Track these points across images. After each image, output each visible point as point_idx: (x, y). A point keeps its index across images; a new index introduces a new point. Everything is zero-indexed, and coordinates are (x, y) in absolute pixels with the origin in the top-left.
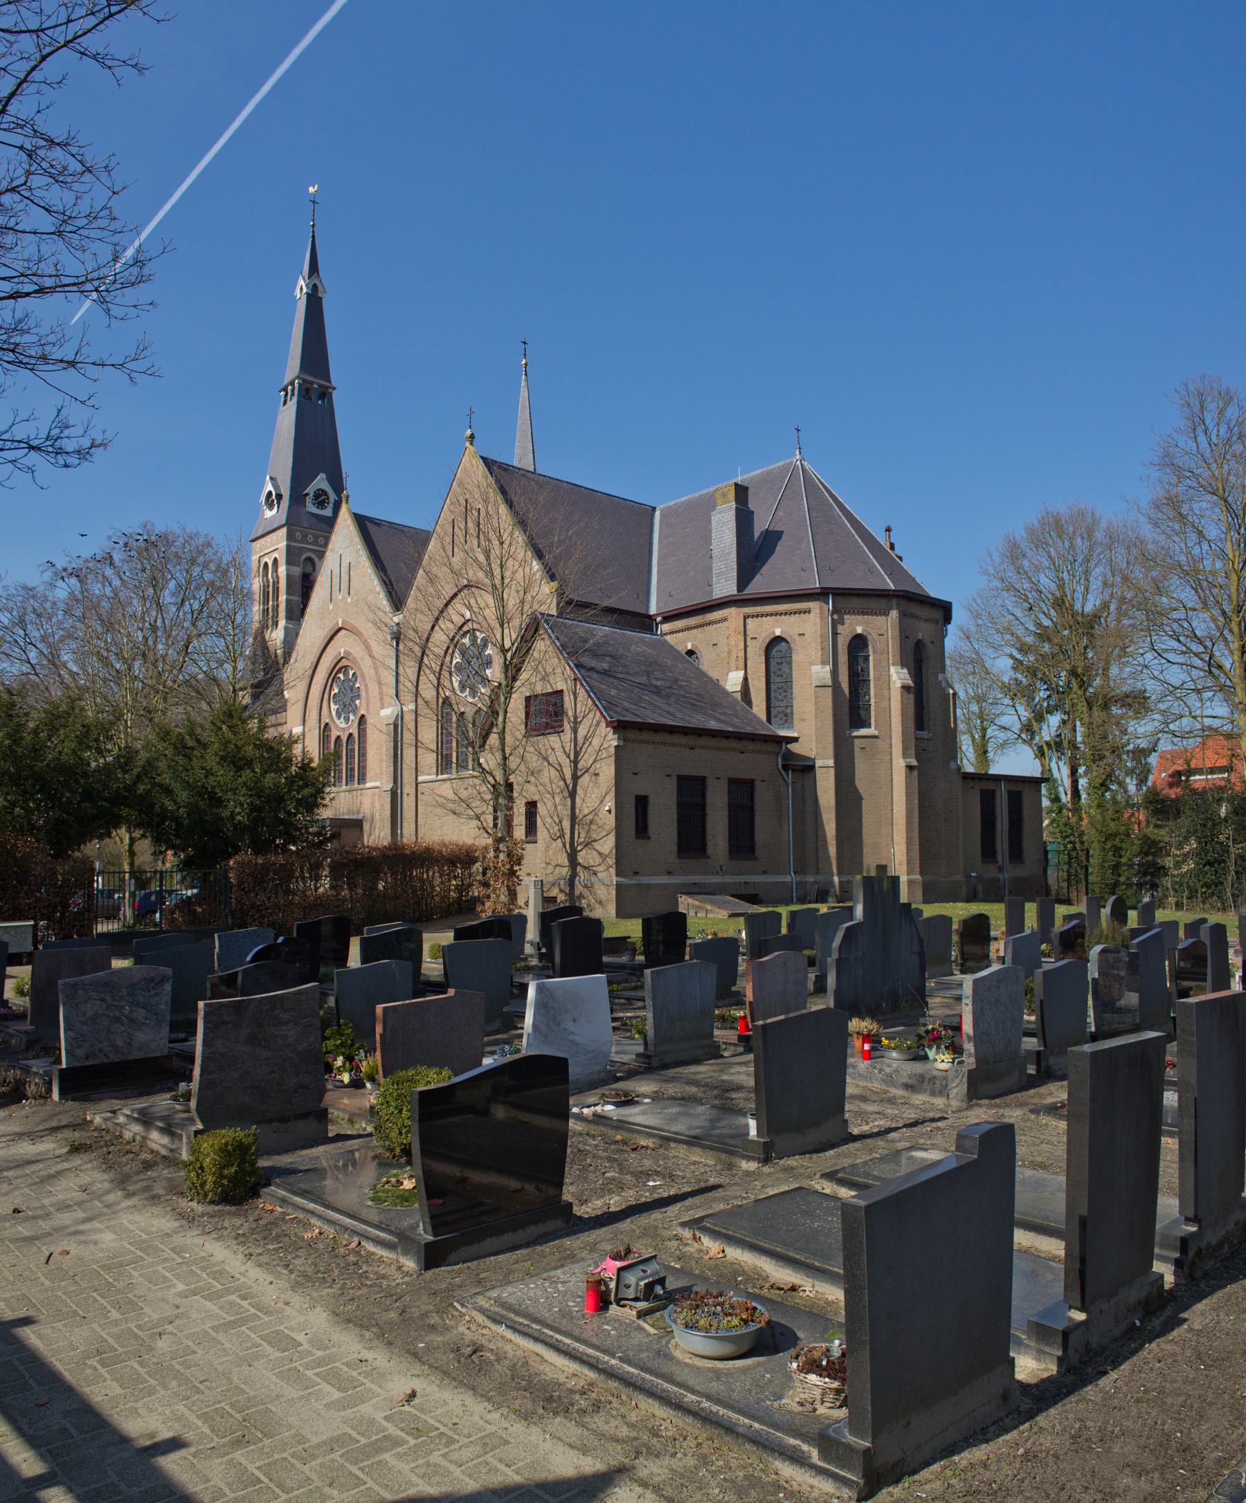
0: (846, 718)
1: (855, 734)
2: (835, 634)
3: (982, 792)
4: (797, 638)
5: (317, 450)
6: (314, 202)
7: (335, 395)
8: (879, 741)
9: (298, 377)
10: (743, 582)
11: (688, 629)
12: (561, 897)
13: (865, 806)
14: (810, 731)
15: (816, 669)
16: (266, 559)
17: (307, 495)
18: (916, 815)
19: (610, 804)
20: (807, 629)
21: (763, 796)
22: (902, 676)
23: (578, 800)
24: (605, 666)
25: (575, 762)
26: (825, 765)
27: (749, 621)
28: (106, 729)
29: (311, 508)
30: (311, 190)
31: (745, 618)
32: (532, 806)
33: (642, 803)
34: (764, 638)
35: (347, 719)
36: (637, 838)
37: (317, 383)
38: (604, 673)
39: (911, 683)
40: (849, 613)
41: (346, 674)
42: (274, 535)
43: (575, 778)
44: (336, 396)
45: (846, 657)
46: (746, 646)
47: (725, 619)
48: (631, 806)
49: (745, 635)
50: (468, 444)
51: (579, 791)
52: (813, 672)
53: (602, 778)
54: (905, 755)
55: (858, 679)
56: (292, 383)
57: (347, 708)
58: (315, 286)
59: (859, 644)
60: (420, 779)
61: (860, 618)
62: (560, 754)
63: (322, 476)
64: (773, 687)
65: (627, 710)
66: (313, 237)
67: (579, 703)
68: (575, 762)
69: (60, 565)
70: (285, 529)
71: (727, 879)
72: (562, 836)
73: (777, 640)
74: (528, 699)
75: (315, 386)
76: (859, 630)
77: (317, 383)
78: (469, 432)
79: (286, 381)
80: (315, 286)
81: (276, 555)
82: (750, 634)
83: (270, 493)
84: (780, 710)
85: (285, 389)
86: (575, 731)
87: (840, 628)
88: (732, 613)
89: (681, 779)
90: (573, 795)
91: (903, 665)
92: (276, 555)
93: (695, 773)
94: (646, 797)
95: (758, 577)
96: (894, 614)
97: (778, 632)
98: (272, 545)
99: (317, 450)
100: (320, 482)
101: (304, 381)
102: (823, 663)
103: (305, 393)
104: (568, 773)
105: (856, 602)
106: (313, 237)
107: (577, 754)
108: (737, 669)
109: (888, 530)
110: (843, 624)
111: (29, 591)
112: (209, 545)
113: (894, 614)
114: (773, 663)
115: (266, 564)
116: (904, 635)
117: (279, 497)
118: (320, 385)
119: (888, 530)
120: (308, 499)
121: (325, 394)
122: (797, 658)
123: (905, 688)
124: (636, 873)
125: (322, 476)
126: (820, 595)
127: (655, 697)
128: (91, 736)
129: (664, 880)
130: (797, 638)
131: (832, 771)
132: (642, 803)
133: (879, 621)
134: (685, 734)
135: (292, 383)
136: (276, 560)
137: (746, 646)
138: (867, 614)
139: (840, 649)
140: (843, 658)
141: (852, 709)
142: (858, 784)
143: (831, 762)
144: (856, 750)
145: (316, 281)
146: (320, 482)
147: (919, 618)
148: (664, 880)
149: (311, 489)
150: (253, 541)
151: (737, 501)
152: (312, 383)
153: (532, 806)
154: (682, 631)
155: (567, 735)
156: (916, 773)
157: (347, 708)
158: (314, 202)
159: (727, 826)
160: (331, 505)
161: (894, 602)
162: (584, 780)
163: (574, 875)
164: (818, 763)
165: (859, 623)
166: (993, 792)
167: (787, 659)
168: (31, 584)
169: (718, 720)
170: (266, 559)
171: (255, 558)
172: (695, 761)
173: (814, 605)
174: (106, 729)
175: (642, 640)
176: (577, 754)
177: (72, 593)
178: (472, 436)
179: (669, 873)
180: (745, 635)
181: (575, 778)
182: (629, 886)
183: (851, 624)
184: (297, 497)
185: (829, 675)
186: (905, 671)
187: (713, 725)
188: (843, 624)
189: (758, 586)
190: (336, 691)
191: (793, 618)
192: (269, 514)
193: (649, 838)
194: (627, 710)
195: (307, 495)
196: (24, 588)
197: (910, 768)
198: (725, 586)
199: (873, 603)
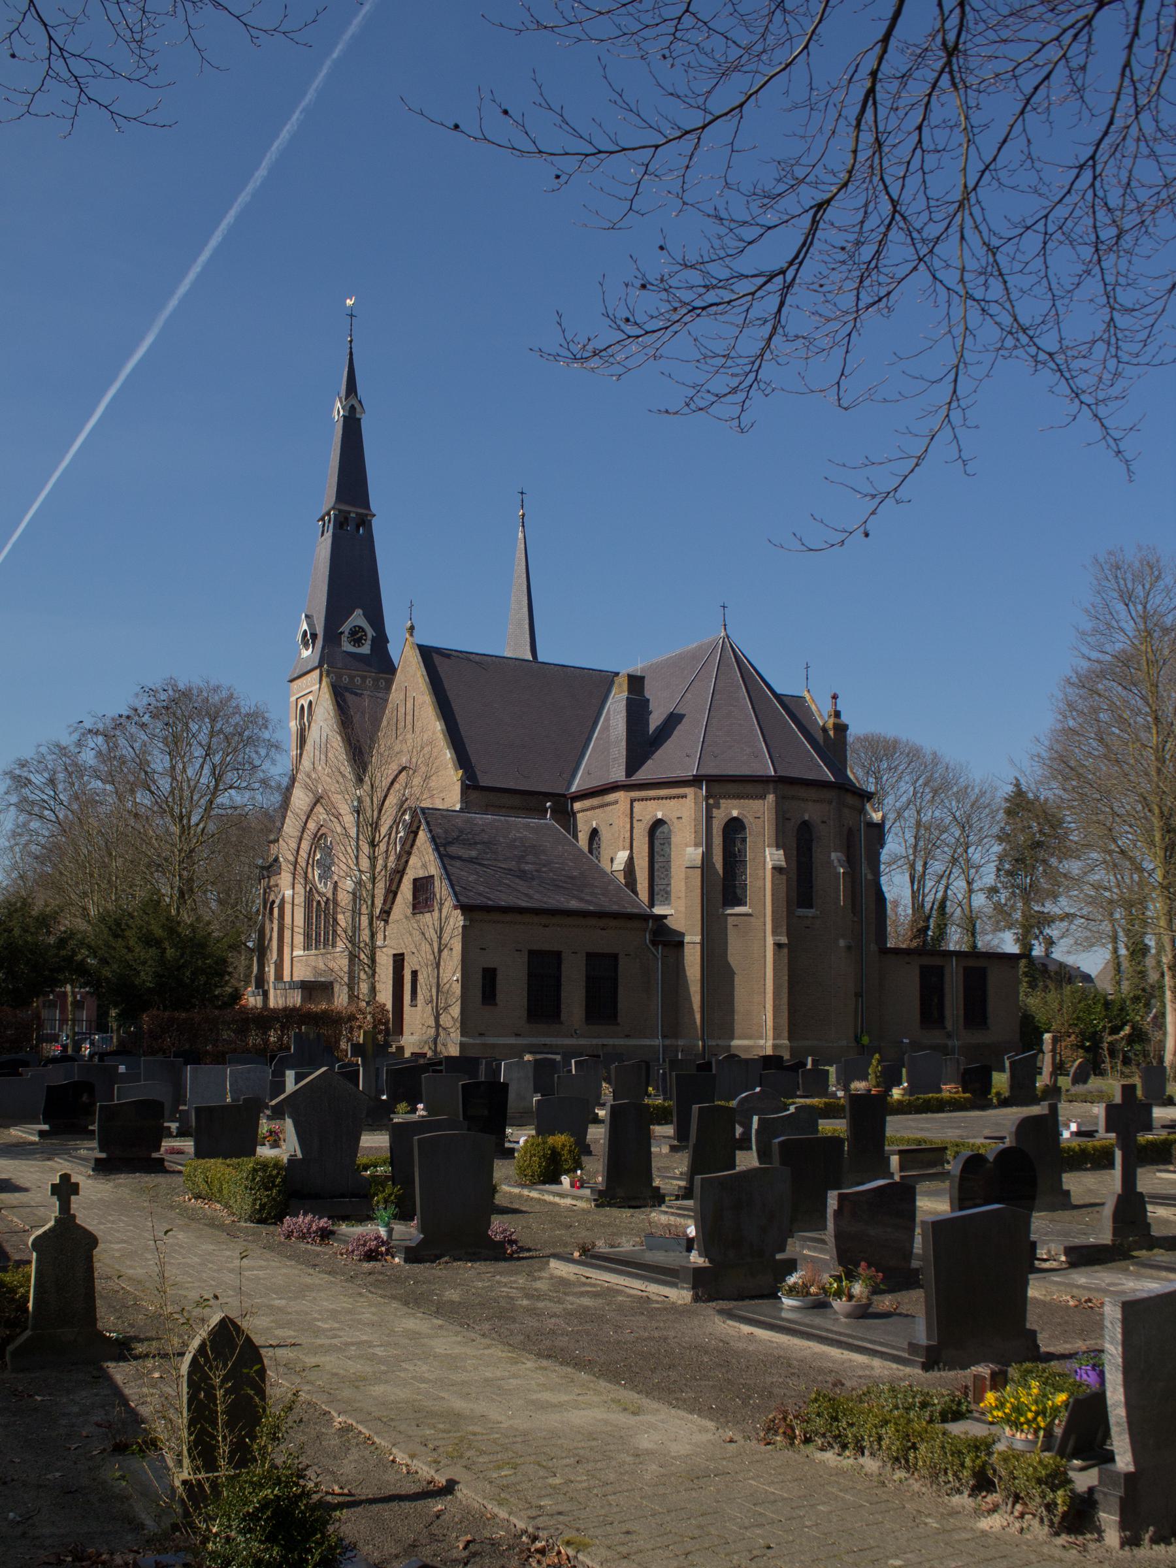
0: (719, 897)
1: (729, 912)
2: (709, 818)
3: (922, 967)
4: (675, 820)
5: (354, 581)
6: (351, 316)
7: (374, 521)
8: (752, 919)
9: (333, 508)
10: (631, 770)
11: (593, 808)
12: (430, 1054)
13: (737, 980)
14: (681, 910)
15: (690, 850)
16: (302, 701)
17: (342, 633)
18: (785, 990)
19: (458, 975)
20: (683, 813)
21: (627, 970)
22: (776, 857)
23: (441, 971)
24: (474, 853)
25: (440, 938)
26: (693, 939)
27: (636, 804)
28: (55, 916)
29: (347, 647)
30: (349, 302)
31: (632, 801)
32: (415, 974)
33: (490, 976)
34: (648, 820)
35: (326, 884)
36: (483, 1004)
37: (354, 512)
38: (471, 860)
39: (783, 864)
40: (725, 797)
41: (326, 840)
42: (308, 677)
43: (440, 951)
44: (376, 523)
45: (721, 839)
46: (632, 828)
47: (616, 802)
48: (477, 978)
49: (632, 818)
50: (408, 636)
51: (442, 963)
52: (686, 852)
53: (454, 952)
54: (774, 933)
55: (734, 860)
56: (328, 514)
57: (326, 875)
58: (353, 408)
59: (734, 827)
60: (295, 954)
61: (735, 802)
62: (432, 931)
63: (358, 612)
64: (656, 866)
65: (480, 894)
66: (351, 354)
67: (441, 889)
68: (440, 938)
69: (88, 725)
70: (318, 671)
71: (583, 1042)
72: (431, 1002)
73: (659, 823)
74: (415, 880)
75: (353, 515)
76: (735, 813)
77: (354, 512)
78: (409, 624)
79: (324, 511)
80: (353, 408)
81: (310, 697)
82: (636, 816)
83: (305, 631)
84: (662, 887)
85: (322, 519)
86: (440, 911)
87: (715, 812)
88: (621, 796)
89: (531, 953)
90: (438, 965)
91: (778, 847)
92: (310, 697)
93: (546, 947)
94: (495, 970)
95: (650, 762)
96: (771, 798)
97: (660, 815)
98: (308, 687)
99: (354, 581)
100: (357, 618)
101: (340, 511)
102: (696, 845)
103: (341, 523)
104: (436, 945)
105: (732, 788)
106: (351, 354)
107: (441, 930)
108: (624, 849)
109: (835, 697)
110: (719, 808)
111: (62, 750)
112: (231, 697)
113: (771, 798)
114: (657, 843)
115: (302, 707)
116: (782, 818)
117: (314, 636)
118: (357, 514)
119: (835, 697)
120: (344, 638)
121: (364, 521)
122: (675, 840)
123: (777, 869)
124: (481, 1035)
125: (358, 612)
126: (695, 781)
127: (517, 881)
128: (45, 921)
129: (512, 1041)
130: (675, 820)
131: (698, 947)
132: (490, 976)
133: (756, 804)
134: (537, 914)
135: (328, 514)
136: (311, 702)
137: (632, 828)
138: (742, 798)
139: (715, 831)
140: (718, 840)
141: (724, 886)
142: (731, 959)
143: (698, 939)
144: (729, 926)
145: (354, 402)
146: (357, 618)
147: (805, 800)
148: (512, 1041)
149: (346, 628)
150: (291, 681)
151: (630, 691)
152: (349, 512)
153: (415, 974)
154: (587, 810)
155: (436, 914)
156: (786, 950)
157: (326, 875)
158: (351, 316)
159: (584, 995)
160: (369, 642)
161: (771, 786)
162: (445, 953)
163: (438, 1035)
164: (687, 939)
165: (734, 807)
166: (942, 968)
167: (667, 841)
168: (64, 743)
169: (581, 900)
170: (302, 701)
171: (293, 699)
172: (547, 938)
173: (689, 791)
174: (55, 916)
175: (527, 826)
176: (441, 930)
177: (100, 753)
178: (412, 628)
179: (517, 1035)
180: (632, 818)
181: (440, 951)
182: (473, 1045)
183: (726, 808)
184: (332, 635)
185: (700, 857)
186: (781, 852)
187: (574, 904)
188: (719, 808)
189: (642, 775)
190: (318, 857)
191: (673, 802)
192: (306, 653)
193: (496, 1005)
194: (480, 894)
195: (342, 633)
196: (58, 745)
197: (778, 946)
198: (618, 773)
199: (749, 788)
